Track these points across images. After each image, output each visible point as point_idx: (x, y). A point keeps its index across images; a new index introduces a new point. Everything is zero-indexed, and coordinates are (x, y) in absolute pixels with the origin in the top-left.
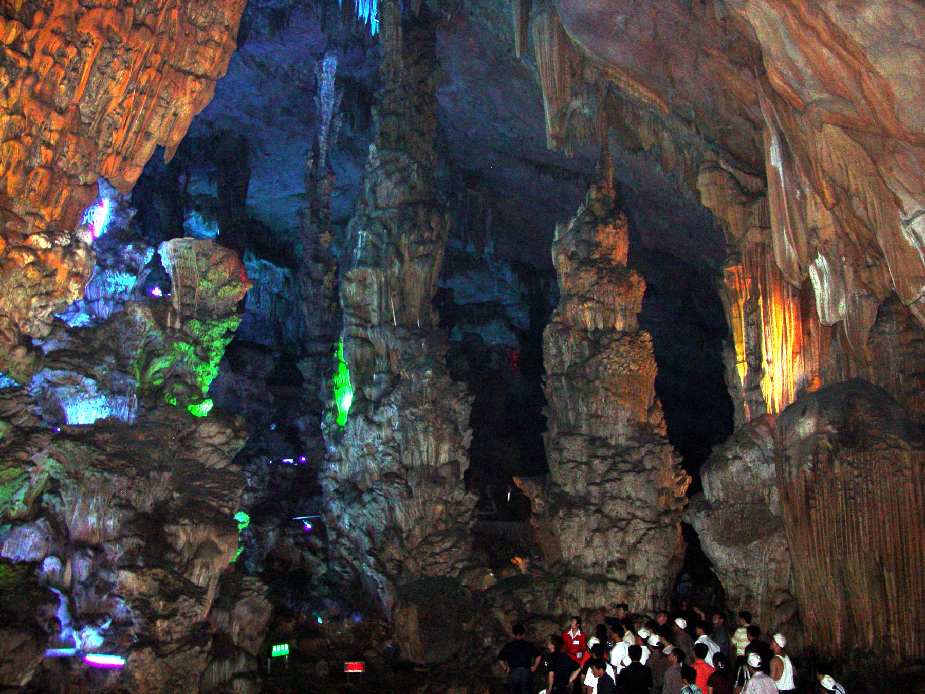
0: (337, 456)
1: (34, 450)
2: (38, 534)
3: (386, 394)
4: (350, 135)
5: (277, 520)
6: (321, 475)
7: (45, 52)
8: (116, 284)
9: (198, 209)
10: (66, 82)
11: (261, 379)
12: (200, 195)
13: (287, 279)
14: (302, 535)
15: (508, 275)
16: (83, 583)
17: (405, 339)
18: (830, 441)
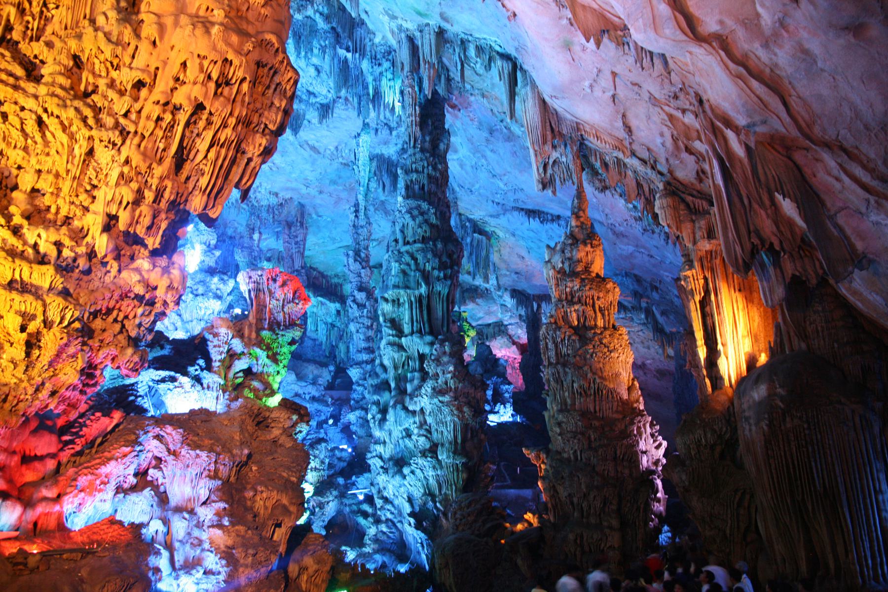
0: (382, 439)
1: (142, 433)
2: (145, 502)
3: (420, 387)
4: (383, 198)
5: (335, 493)
6: (369, 455)
8: (206, 308)
10: (163, 141)
11: (320, 385)
13: (338, 312)
14: (355, 504)
15: (509, 301)
16: (180, 541)
17: (432, 344)
18: (781, 401)
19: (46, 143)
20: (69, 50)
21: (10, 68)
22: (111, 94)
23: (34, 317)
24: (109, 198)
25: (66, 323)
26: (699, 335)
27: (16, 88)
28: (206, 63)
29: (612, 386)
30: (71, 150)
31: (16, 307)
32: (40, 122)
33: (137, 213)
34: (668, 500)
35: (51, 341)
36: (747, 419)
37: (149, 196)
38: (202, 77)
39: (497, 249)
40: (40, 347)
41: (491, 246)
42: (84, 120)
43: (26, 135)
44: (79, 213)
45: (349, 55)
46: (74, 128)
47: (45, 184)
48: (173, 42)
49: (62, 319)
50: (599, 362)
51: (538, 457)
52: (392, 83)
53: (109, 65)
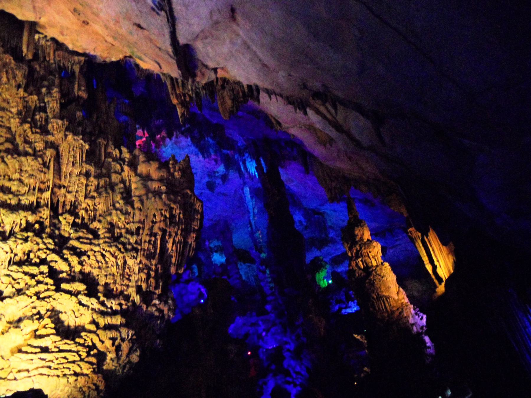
7: (145, 242)
9: (216, 252)
12: (216, 246)
19: (107, 263)
20: (107, 221)
21: (87, 236)
22: (128, 236)
23: (116, 339)
24: (136, 279)
25: (130, 337)
26: (425, 259)
27: (91, 244)
28: (163, 212)
30: (117, 263)
31: (109, 336)
32: (103, 256)
33: (149, 282)
34: (435, 346)
35: (125, 347)
37: (152, 274)
38: (163, 218)
40: (121, 351)
42: (119, 250)
43: (98, 261)
44: (125, 288)
45: (228, 152)
46: (116, 254)
47: (110, 281)
48: (148, 207)
49: (128, 336)
51: (362, 338)
52: (251, 163)
53: (124, 223)
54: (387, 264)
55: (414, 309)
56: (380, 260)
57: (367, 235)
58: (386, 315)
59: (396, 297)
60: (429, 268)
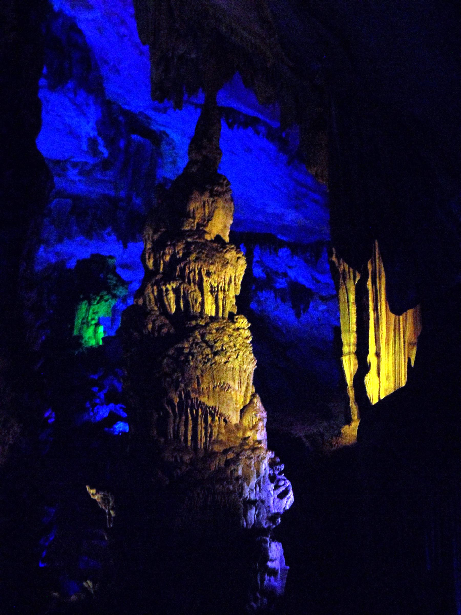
29: (211, 404)
36: (100, 503)
39: (170, 159)
41: (160, 155)
50: (196, 368)
54: (243, 322)
55: (272, 464)
56: (231, 305)
57: (221, 224)
58: (187, 458)
59: (235, 419)
60: (349, 366)
